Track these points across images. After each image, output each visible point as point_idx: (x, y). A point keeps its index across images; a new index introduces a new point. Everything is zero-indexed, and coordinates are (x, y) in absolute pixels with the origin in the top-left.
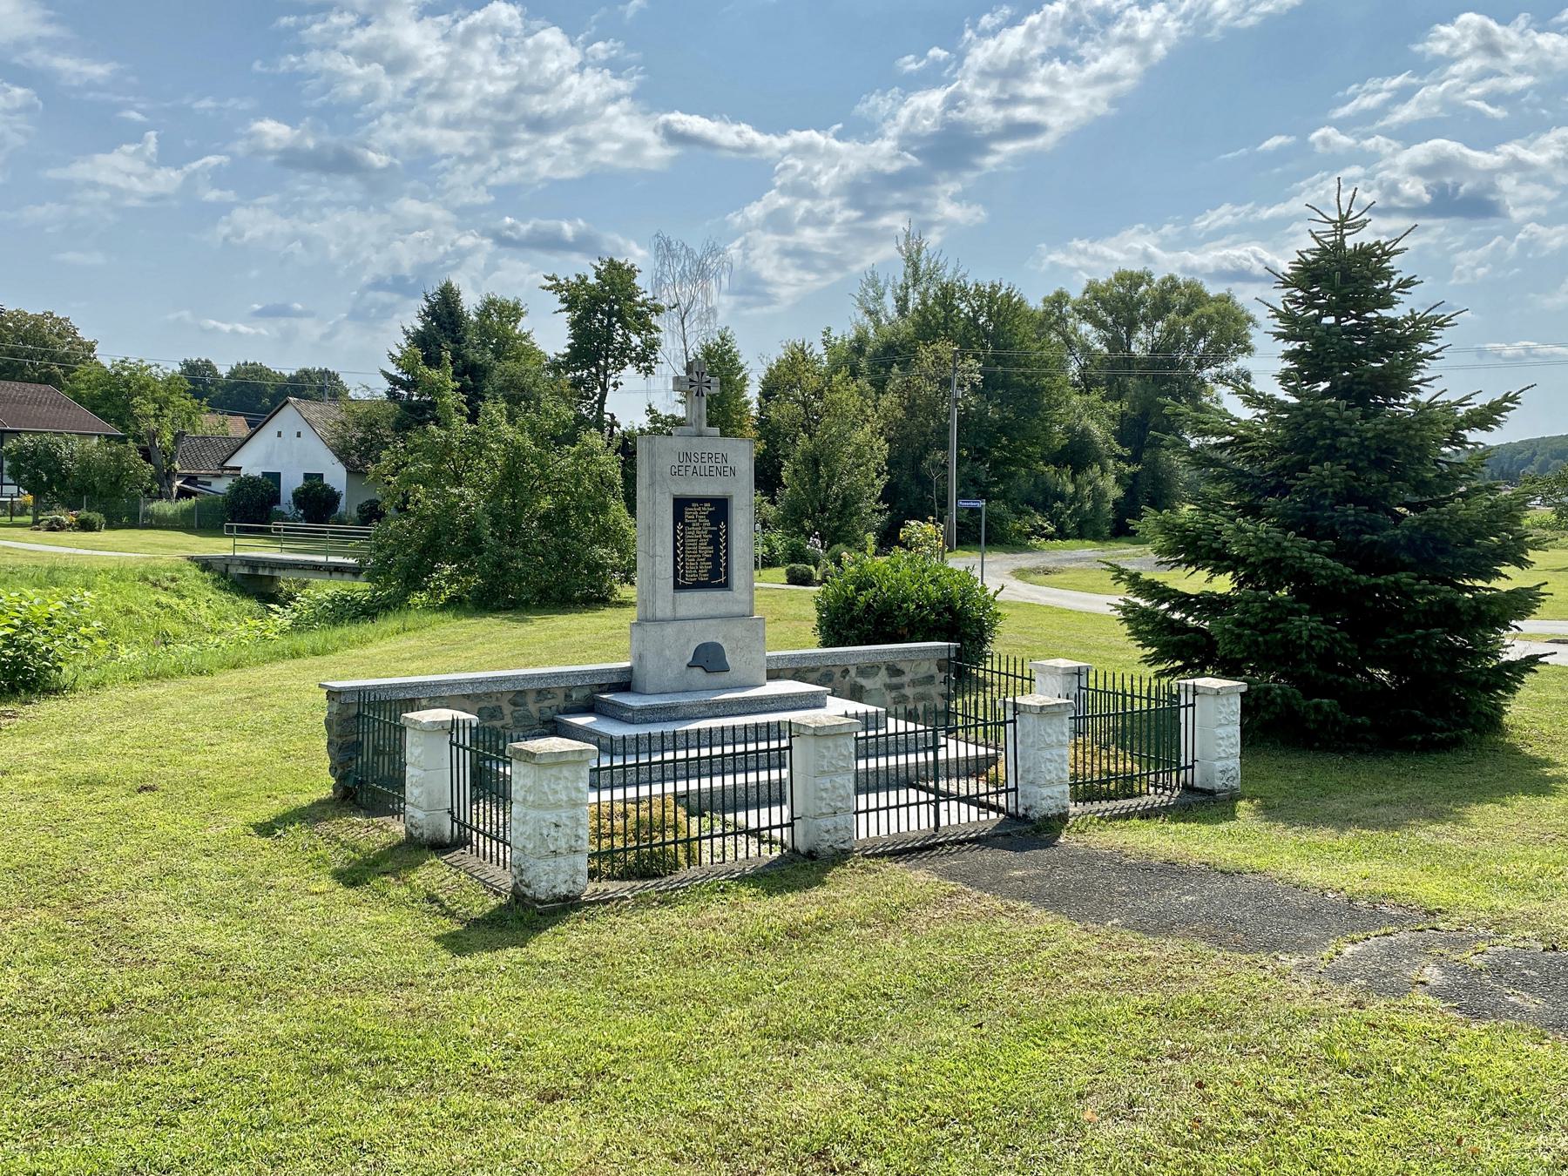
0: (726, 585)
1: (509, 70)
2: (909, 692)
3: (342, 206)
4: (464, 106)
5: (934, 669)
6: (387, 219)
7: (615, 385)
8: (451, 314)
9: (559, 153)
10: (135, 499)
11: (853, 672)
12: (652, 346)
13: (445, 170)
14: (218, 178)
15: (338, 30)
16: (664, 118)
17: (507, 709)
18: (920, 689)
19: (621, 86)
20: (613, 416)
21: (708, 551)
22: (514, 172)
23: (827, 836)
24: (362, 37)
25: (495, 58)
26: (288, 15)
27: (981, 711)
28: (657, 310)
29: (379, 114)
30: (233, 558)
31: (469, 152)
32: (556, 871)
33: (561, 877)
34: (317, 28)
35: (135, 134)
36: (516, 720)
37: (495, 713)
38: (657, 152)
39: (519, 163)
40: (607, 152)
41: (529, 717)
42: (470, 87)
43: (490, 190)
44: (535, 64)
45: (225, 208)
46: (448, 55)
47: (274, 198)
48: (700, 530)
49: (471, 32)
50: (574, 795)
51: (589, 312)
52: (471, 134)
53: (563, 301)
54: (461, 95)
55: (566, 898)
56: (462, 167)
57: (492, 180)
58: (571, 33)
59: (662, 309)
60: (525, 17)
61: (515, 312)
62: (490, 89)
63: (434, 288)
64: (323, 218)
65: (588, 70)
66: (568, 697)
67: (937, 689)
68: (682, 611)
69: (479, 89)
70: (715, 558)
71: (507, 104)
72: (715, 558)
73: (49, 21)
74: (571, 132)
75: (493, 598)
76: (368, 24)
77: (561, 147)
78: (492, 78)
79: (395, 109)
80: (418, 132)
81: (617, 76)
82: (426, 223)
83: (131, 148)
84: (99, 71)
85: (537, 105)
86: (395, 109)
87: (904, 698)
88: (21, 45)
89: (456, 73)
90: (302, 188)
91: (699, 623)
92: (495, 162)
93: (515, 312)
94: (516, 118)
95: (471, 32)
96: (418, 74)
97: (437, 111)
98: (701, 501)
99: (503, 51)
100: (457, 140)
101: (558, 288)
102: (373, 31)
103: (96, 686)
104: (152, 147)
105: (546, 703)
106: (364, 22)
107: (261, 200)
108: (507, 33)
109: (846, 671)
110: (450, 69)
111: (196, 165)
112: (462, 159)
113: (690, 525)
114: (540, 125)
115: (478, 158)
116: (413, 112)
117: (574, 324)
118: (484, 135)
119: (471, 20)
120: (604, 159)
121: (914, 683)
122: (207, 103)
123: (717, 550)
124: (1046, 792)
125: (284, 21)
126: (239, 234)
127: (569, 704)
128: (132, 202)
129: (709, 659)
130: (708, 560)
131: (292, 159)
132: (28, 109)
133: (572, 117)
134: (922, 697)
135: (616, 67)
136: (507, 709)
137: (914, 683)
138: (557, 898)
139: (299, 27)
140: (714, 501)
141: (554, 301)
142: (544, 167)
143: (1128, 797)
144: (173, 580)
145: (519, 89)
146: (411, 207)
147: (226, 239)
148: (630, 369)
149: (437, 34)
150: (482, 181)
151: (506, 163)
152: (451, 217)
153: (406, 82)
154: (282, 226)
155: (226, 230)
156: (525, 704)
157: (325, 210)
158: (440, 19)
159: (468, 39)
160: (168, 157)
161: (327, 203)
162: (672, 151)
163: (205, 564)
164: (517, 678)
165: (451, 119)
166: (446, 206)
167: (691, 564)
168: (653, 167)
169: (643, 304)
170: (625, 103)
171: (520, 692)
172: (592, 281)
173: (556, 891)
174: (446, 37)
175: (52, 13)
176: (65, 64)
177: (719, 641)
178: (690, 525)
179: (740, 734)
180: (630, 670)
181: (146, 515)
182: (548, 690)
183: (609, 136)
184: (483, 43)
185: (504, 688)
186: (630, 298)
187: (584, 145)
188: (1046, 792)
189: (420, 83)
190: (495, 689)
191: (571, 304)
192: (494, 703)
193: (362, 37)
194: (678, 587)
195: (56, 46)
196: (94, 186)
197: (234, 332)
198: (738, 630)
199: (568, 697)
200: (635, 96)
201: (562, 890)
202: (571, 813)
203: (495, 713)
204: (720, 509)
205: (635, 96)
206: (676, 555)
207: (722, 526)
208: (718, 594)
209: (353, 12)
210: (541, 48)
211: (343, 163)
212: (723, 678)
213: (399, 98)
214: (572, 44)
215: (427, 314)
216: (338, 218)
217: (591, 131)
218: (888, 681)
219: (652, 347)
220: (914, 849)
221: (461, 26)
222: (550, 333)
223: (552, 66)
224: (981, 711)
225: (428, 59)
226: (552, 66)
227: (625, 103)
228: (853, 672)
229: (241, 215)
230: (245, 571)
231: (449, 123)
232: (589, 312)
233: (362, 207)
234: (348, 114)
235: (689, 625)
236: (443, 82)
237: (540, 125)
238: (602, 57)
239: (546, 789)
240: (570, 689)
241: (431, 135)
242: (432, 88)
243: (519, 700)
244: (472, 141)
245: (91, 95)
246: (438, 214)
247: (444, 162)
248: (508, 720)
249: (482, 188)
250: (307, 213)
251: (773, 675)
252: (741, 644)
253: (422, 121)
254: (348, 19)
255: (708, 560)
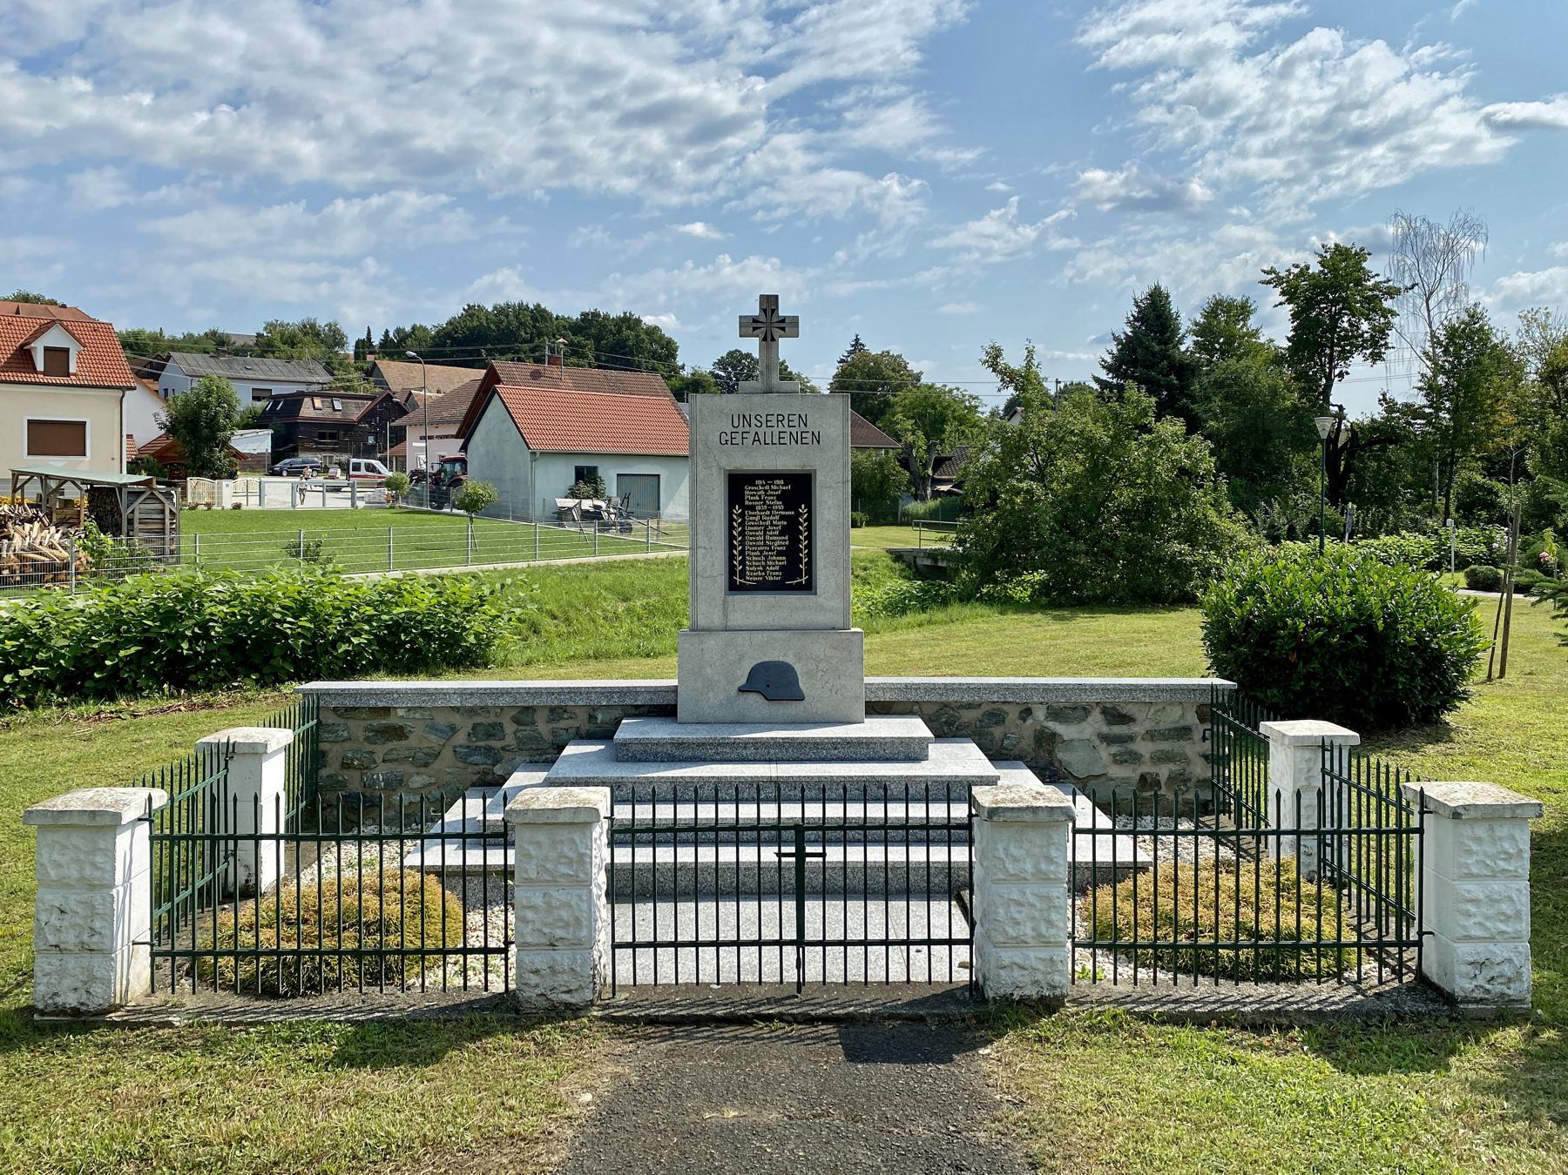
0: (809, 587)
1: (1329, 91)
2: (1144, 748)
3: (1170, 240)
4: (1283, 133)
5: (1191, 718)
6: (1211, 246)
7: (1341, 375)
8: (1159, 317)
9: (1382, 162)
10: (895, 500)
11: (1040, 713)
12: (1381, 332)
13: (1266, 194)
14: (1065, 228)
15: (1164, 87)
16: (1490, 109)
17: (510, 728)
18: (1166, 746)
19: (1450, 85)
20: (1341, 408)
21: (781, 542)
22: (1336, 188)
23: (534, 979)
24: (1184, 88)
25: (1314, 82)
26: (1120, 82)
27: (1364, 778)
28: (1392, 293)
29: (1202, 155)
30: (920, 551)
31: (1290, 174)
32: (62, 973)
33: (67, 982)
34: (1146, 87)
35: (1001, 201)
36: (520, 741)
37: (494, 731)
38: (1490, 146)
39: (1338, 178)
40: (1433, 155)
41: (537, 738)
42: (1289, 114)
43: (1312, 207)
44: (1357, 81)
45: (1067, 255)
46: (1266, 89)
47: (1111, 240)
48: (768, 513)
49: (1290, 64)
50: (88, 872)
51: (1310, 303)
52: (1293, 158)
53: (1283, 293)
54: (1280, 124)
55: (76, 1012)
56: (1282, 190)
57: (1313, 198)
58: (1395, 46)
59: (1398, 291)
60: (1346, 39)
61: (1244, 310)
62: (1307, 113)
63: (1142, 292)
64: (1154, 252)
65: (1416, 77)
66: (592, 717)
67: (1195, 748)
68: (737, 619)
69: (1297, 114)
70: (792, 552)
71: (1325, 125)
72: (792, 552)
73: (933, 123)
74: (1393, 141)
75: (1064, 597)
76: (1191, 75)
77: (1383, 157)
78: (1310, 103)
79: (1216, 147)
80: (1241, 165)
81: (1445, 74)
82: (1249, 245)
83: (995, 213)
84: (968, 156)
85: (1356, 120)
86: (1216, 147)
87: (1135, 758)
88: (913, 146)
89: (1274, 105)
90: (1134, 228)
91: (758, 636)
92: (1315, 180)
93: (1244, 310)
94: (1336, 134)
95: (1290, 64)
96: (1237, 112)
97: (1256, 142)
98: (769, 477)
99: (1321, 74)
100: (1276, 166)
101: (1278, 281)
102: (1195, 81)
103: (529, 663)
104: (1013, 211)
105: (562, 724)
106: (1188, 74)
107: (1098, 244)
108: (1327, 57)
109: (1027, 712)
110: (1268, 102)
111: (1049, 220)
112: (1283, 182)
113: (753, 508)
114: (1361, 139)
115: (1299, 179)
116: (1234, 149)
117: (1295, 316)
118: (1302, 158)
119: (1287, 54)
120: (1429, 162)
121: (1152, 735)
122: (1052, 169)
123: (794, 542)
124: (1007, 956)
125: (1117, 87)
126: (1081, 273)
127: (592, 727)
128: (997, 258)
129: (773, 683)
130: (780, 553)
131: (1128, 205)
132: (920, 194)
133: (1401, 123)
134: (1162, 758)
135: (1442, 68)
136: (510, 728)
137: (1152, 735)
138: (61, 1011)
139: (1128, 91)
140: (788, 477)
141: (1275, 295)
142: (1365, 178)
143: (1273, 978)
144: (865, 569)
145: (1339, 108)
146: (1237, 232)
147: (1071, 280)
148: (1357, 358)
149: (1257, 71)
150: (1301, 200)
151: (1326, 180)
152: (1270, 236)
153: (1226, 120)
154: (1118, 263)
155: (1070, 273)
156: (533, 723)
157: (1155, 245)
158: (1260, 57)
159: (1286, 72)
160: (1028, 215)
161: (1157, 239)
162: (1506, 142)
163: (897, 556)
164: (518, 691)
165: (1271, 147)
166: (1267, 226)
167: (753, 559)
168: (1484, 161)
169: (1376, 286)
170: (1455, 102)
171: (527, 708)
172: (1315, 268)
173: (59, 1000)
174: (1265, 74)
175: (936, 116)
176: (944, 155)
177: (790, 660)
178: (753, 508)
179: (707, 792)
180: (675, 690)
181: (905, 514)
182: (564, 709)
183: (1434, 139)
184: (1302, 71)
185: (501, 702)
186: (1358, 282)
187: (1408, 150)
188: (1007, 956)
189: (1239, 119)
190: (490, 702)
191: (1290, 294)
192: (492, 719)
193: (1184, 88)
194: (733, 587)
195: (935, 142)
196: (967, 249)
197: (1079, 360)
198: (819, 646)
199: (592, 717)
200: (1465, 93)
201: (71, 1000)
202: (86, 896)
203: (494, 731)
204: (799, 488)
205: (1465, 93)
206: (731, 547)
207: (803, 509)
208: (793, 599)
209: (1177, 68)
210: (1360, 66)
211: (1168, 202)
212: (793, 709)
213: (1220, 137)
214: (1397, 55)
215: (1136, 319)
216: (1168, 251)
217: (1416, 134)
218: (1105, 729)
219: (1382, 332)
220: (698, 1021)
221: (1279, 61)
222: (1275, 326)
223: (1372, 80)
224: (1364, 778)
225: (1247, 97)
226: (1372, 80)
227: (1455, 102)
228: (1040, 713)
229: (1085, 258)
230: (928, 562)
231: (1269, 152)
232: (1310, 303)
233: (1189, 238)
234: (1179, 160)
235: (741, 638)
236: (1262, 114)
237: (1361, 139)
238: (1428, 61)
239: (44, 860)
240: (594, 708)
241: (1253, 164)
242: (1250, 123)
243: (525, 718)
244: (1292, 165)
245: (963, 177)
246: (1260, 235)
247: (1267, 188)
248: (510, 740)
249: (1304, 206)
250: (1139, 250)
251: (877, 708)
252: (823, 665)
253: (1243, 154)
254: (1175, 74)
255: (780, 553)
